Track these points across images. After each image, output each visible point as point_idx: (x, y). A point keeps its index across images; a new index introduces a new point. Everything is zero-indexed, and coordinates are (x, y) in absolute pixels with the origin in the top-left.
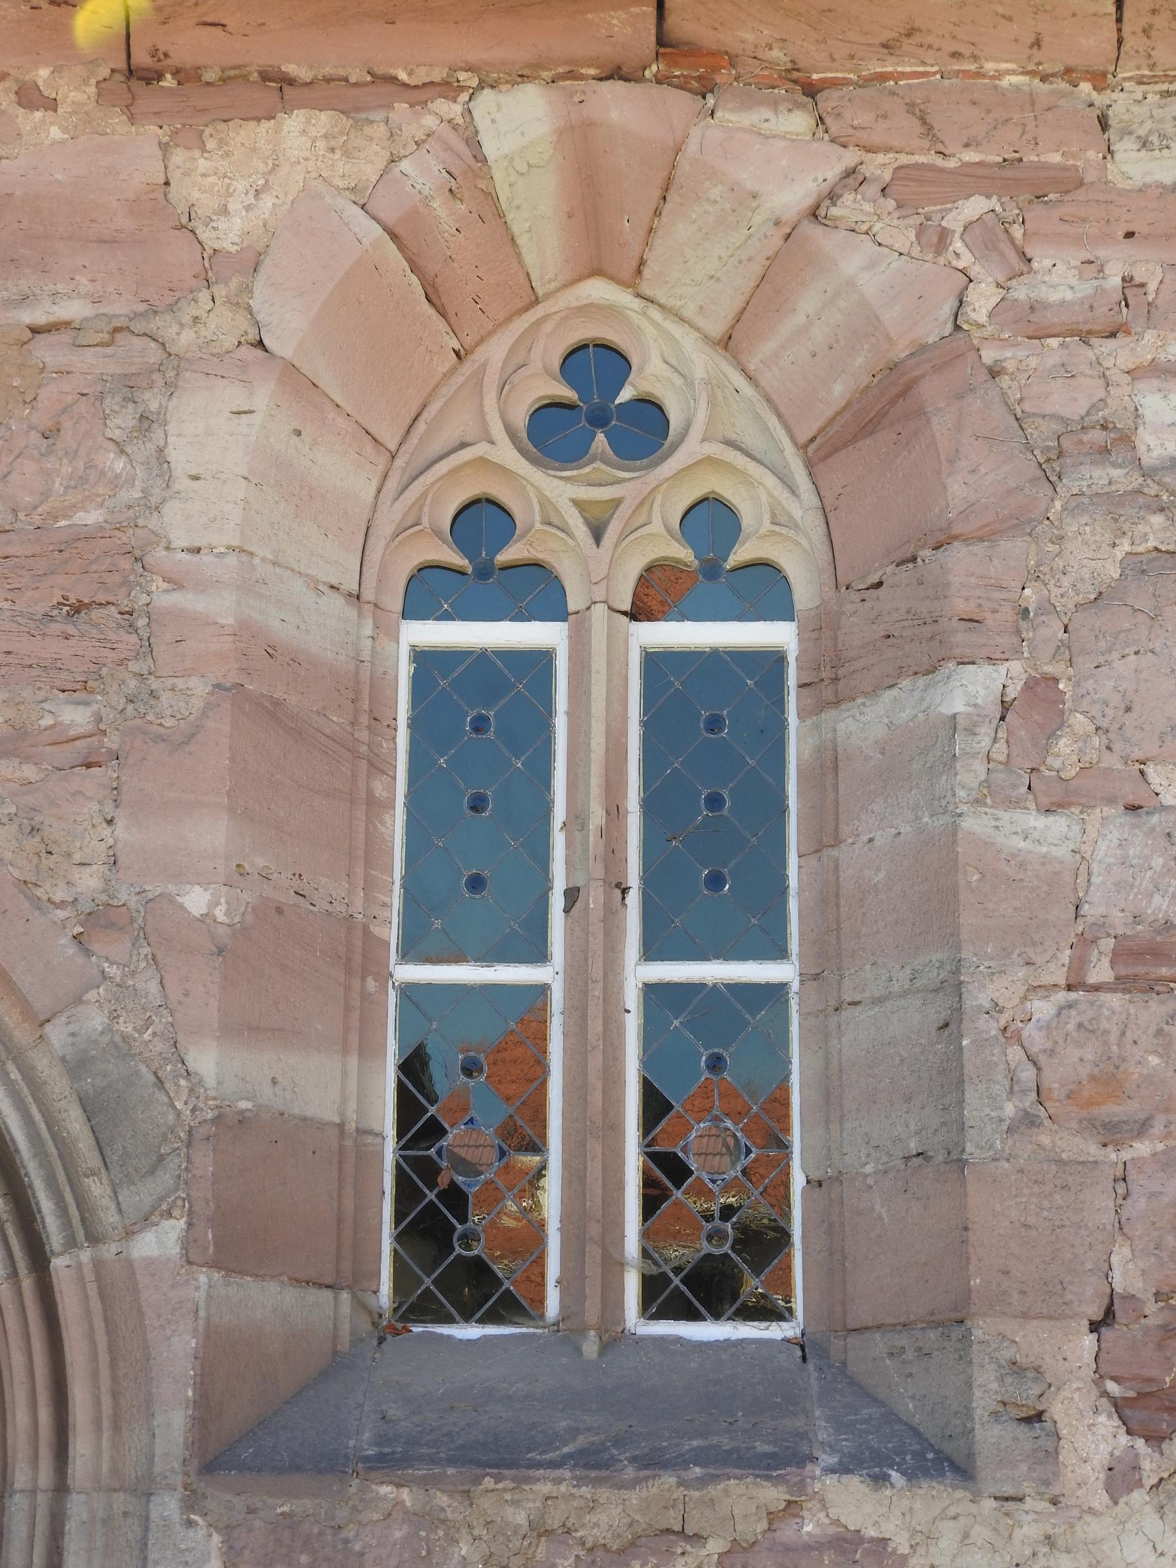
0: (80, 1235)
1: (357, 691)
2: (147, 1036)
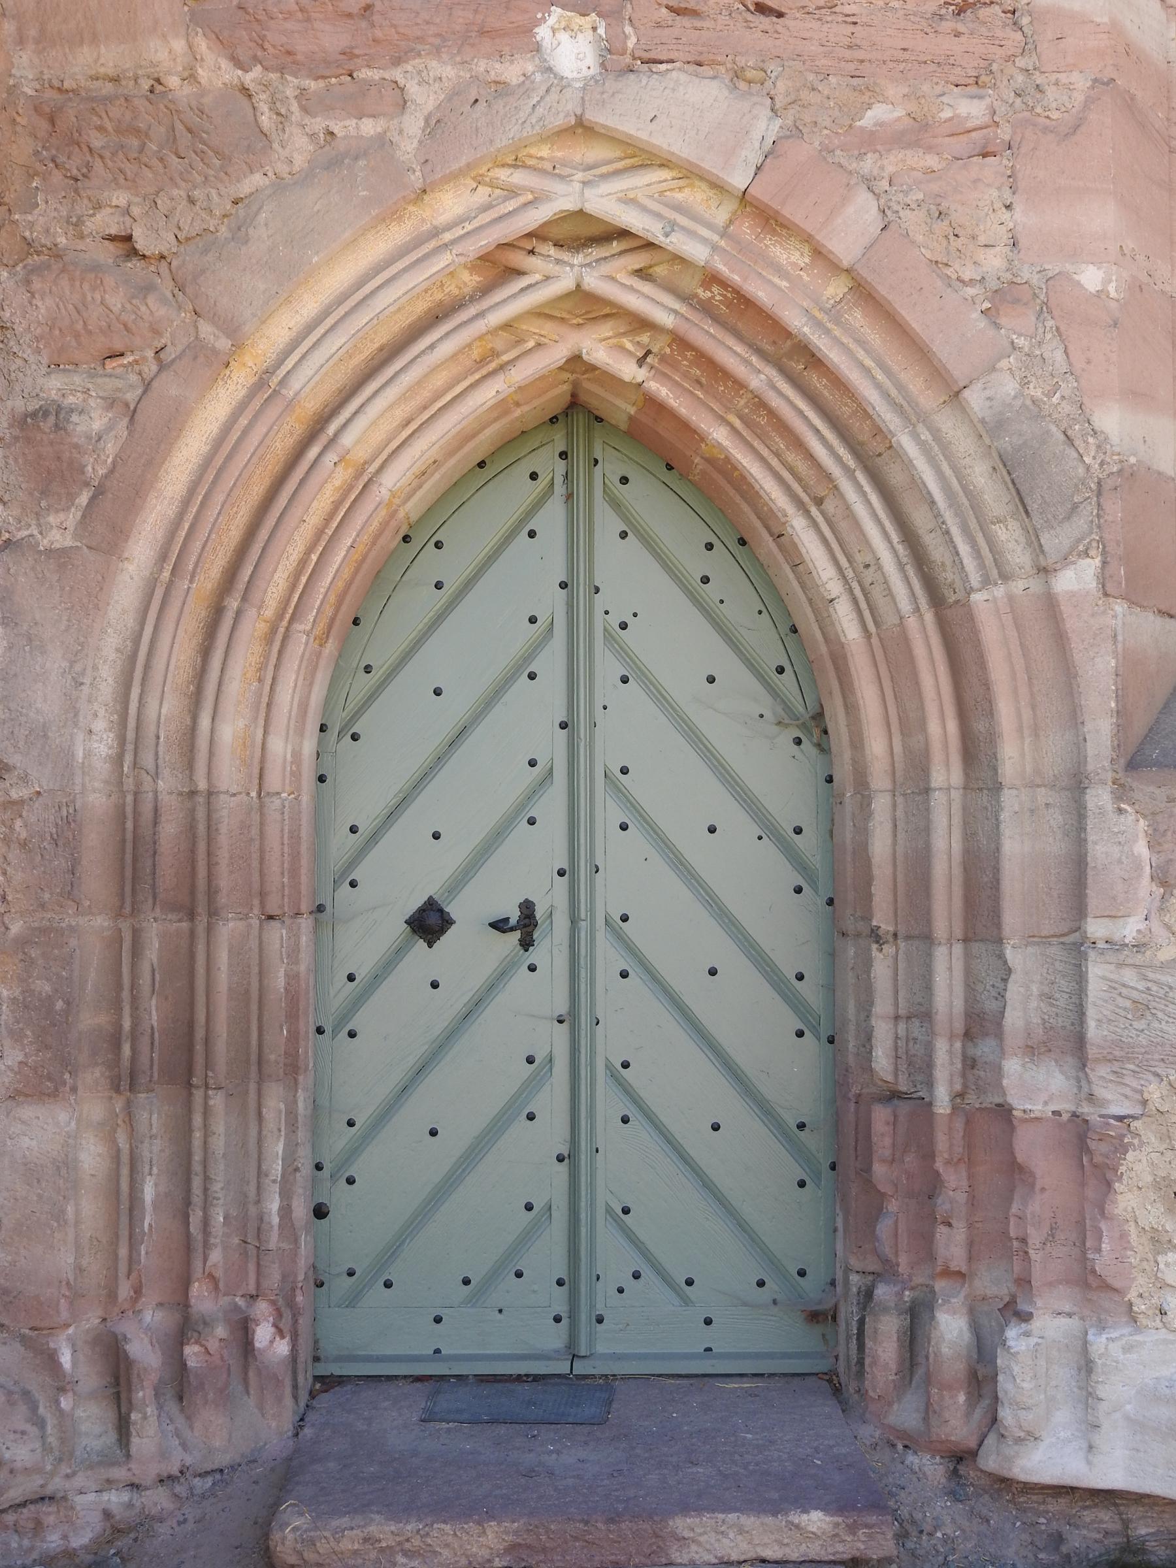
0: (994, 573)
2: (1055, 400)
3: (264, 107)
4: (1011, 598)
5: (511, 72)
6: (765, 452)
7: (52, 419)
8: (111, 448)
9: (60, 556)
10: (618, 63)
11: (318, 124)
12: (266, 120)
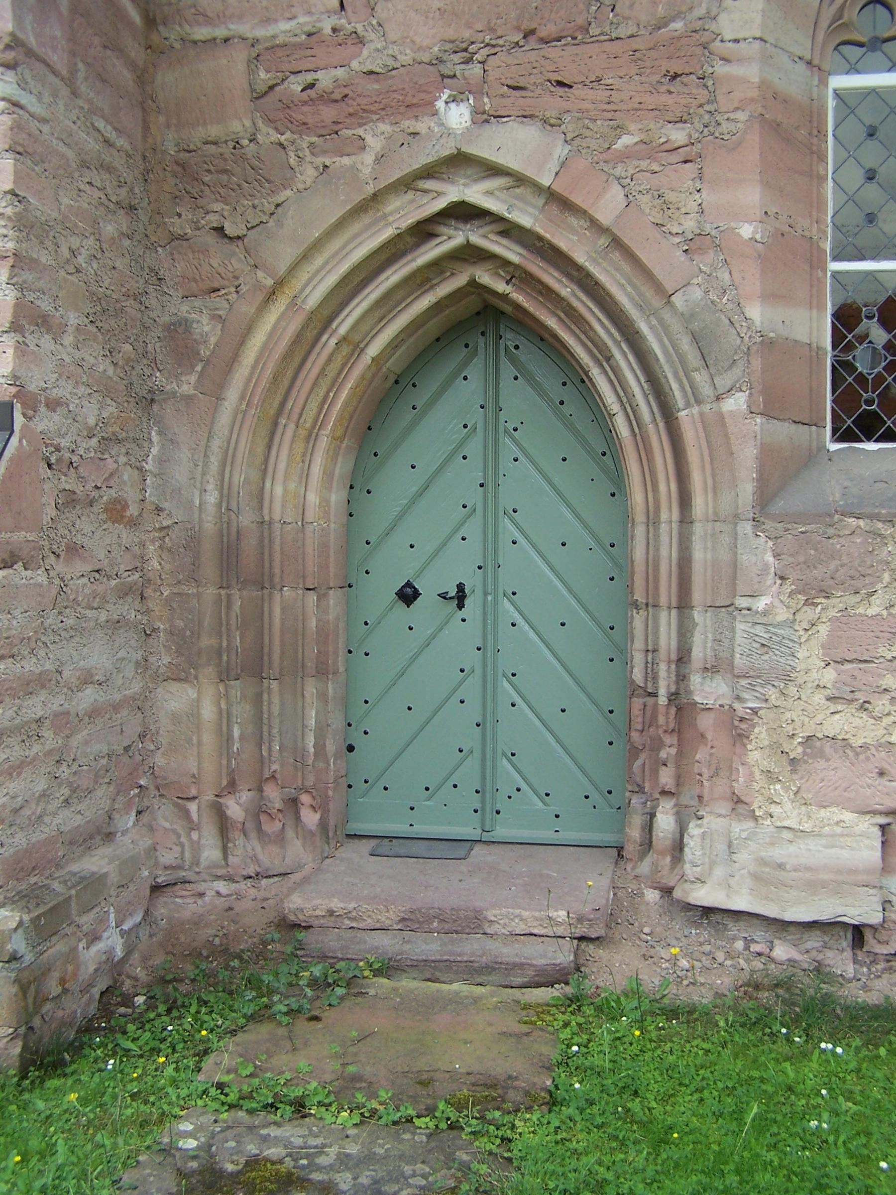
0: (692, 400)
1: (811, 117)
2: (724, 300)
3: (292, 154)
4: (701, 414)
5: (421, 126)
6: (578, 332)
7: (183, 327)
8: (213, 340)
9: (188, 399)
10: (483, 118)
11: (320, 161)
12: (293, 161)
